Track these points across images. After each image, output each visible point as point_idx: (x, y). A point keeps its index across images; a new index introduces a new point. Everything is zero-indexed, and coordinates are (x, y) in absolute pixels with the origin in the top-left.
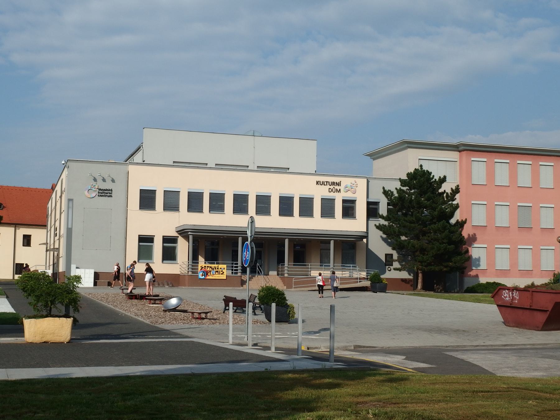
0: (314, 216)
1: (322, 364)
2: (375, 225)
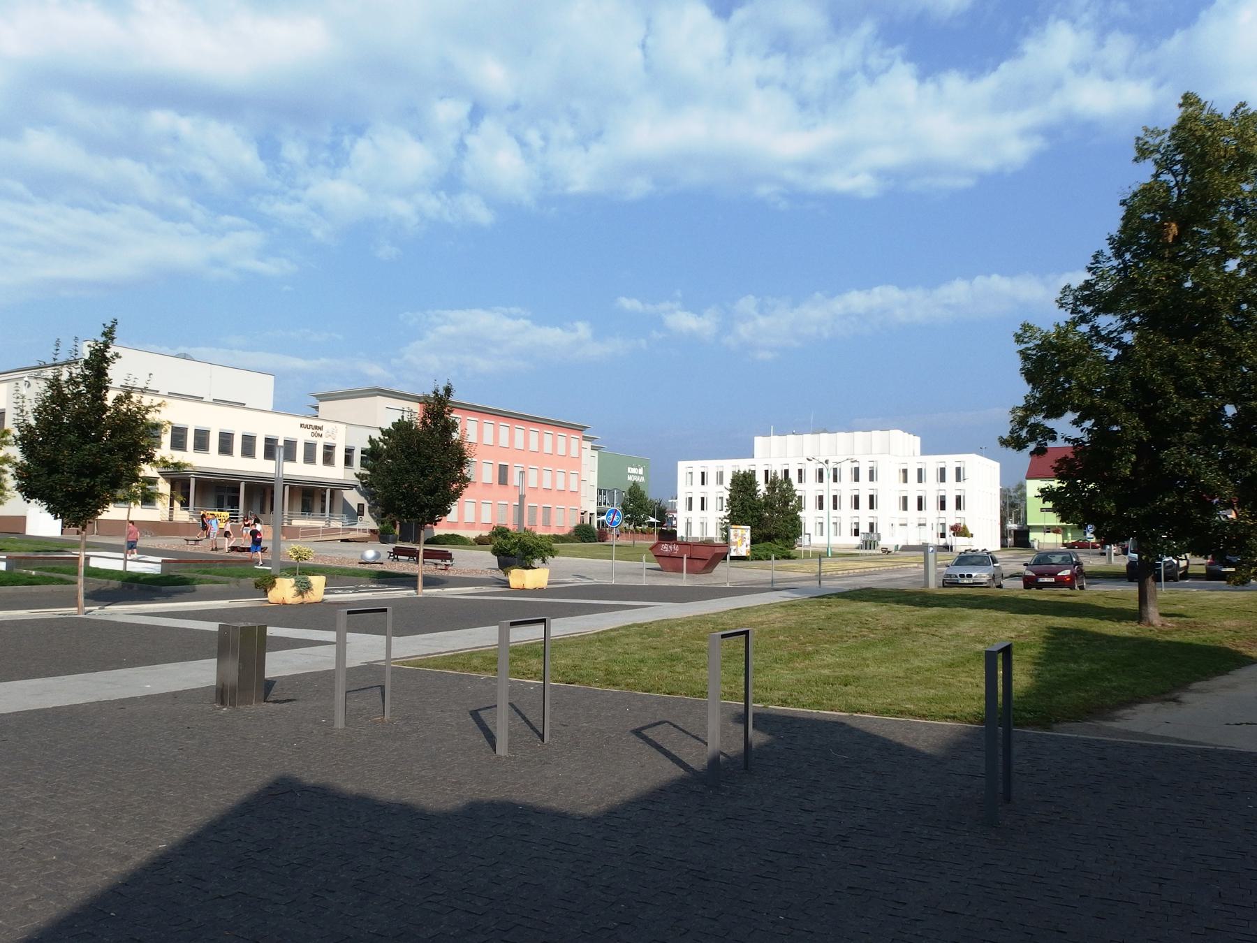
0: (256, 456)
1: (991, 616)
2: (355, 474)
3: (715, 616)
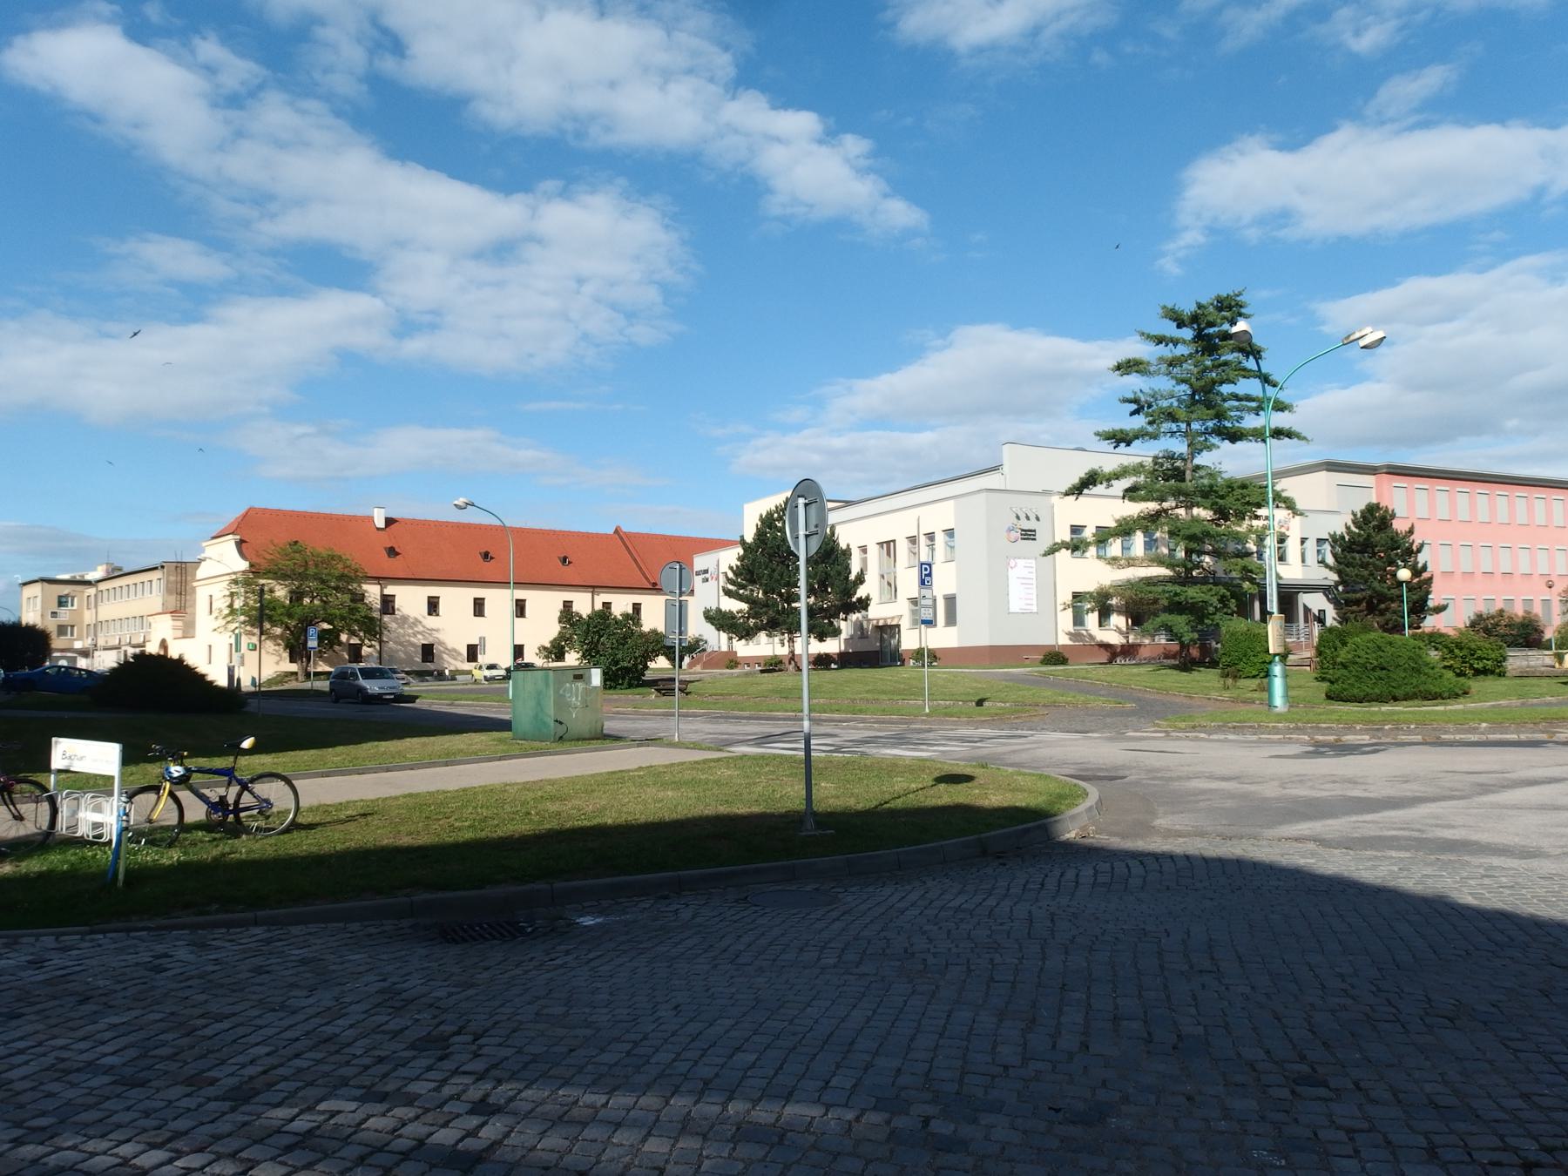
0: (527, 615)
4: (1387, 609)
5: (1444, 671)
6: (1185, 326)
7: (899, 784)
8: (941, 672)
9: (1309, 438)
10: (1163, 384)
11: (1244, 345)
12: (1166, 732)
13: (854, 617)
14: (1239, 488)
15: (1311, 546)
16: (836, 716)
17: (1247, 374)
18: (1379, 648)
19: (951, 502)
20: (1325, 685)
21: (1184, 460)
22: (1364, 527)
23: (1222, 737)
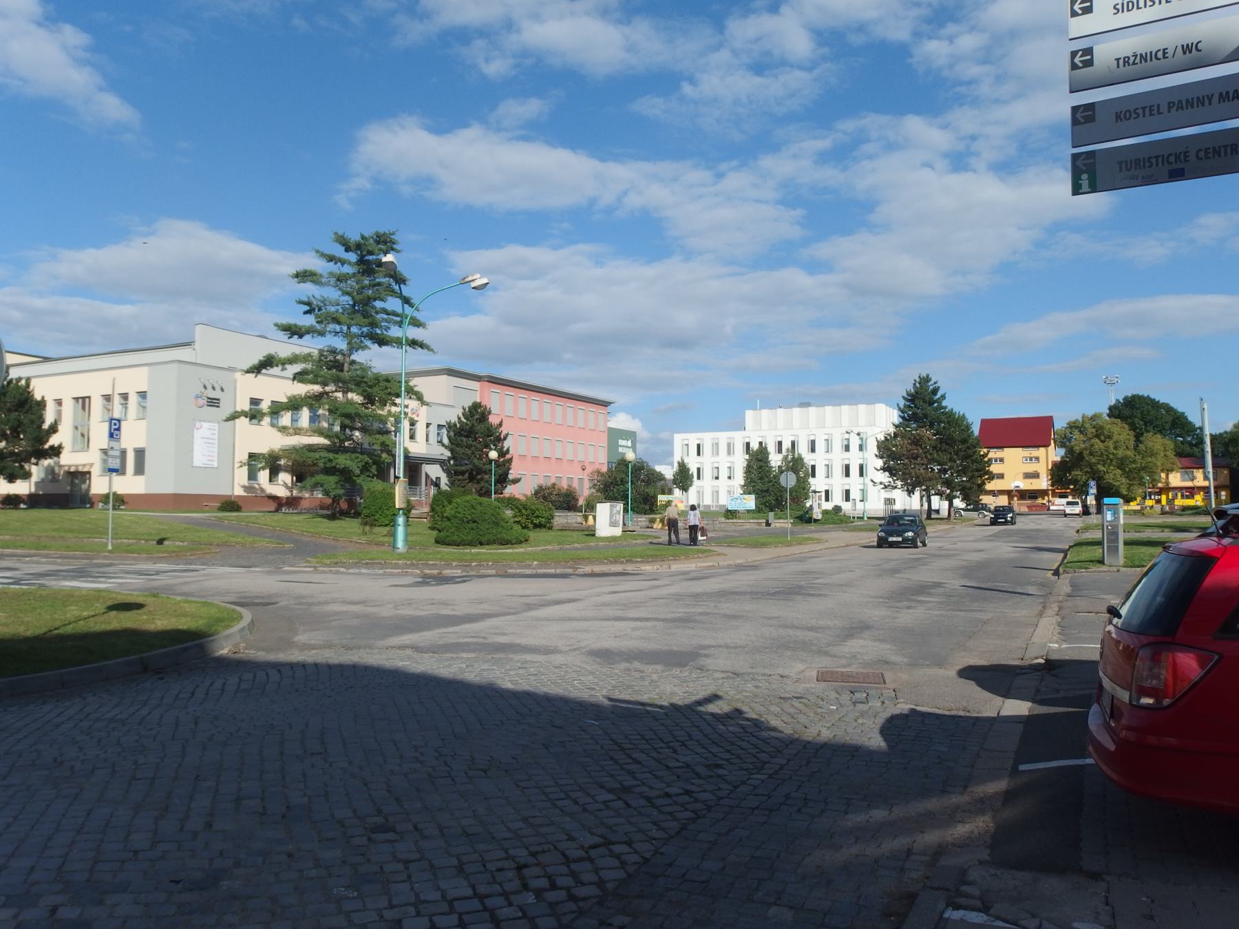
3: (483, 572)
4: (482, 479)
5: (513, 525)
6: (351, 251)
7: (73, 612)
8: (126, 514)
9: (435, 350)
10: (332, 293)
11: (392, 273)
12: (314, 567)
13: (47, 462)
14: (383, 381)
15: (433, 429)
16: (19, 551)
17: (393, 292)
18: (473, 506)
19: (146, 369)
20: (435, 533)
21: (344, 355)
22: (471, 419)
23: (357, 571)
